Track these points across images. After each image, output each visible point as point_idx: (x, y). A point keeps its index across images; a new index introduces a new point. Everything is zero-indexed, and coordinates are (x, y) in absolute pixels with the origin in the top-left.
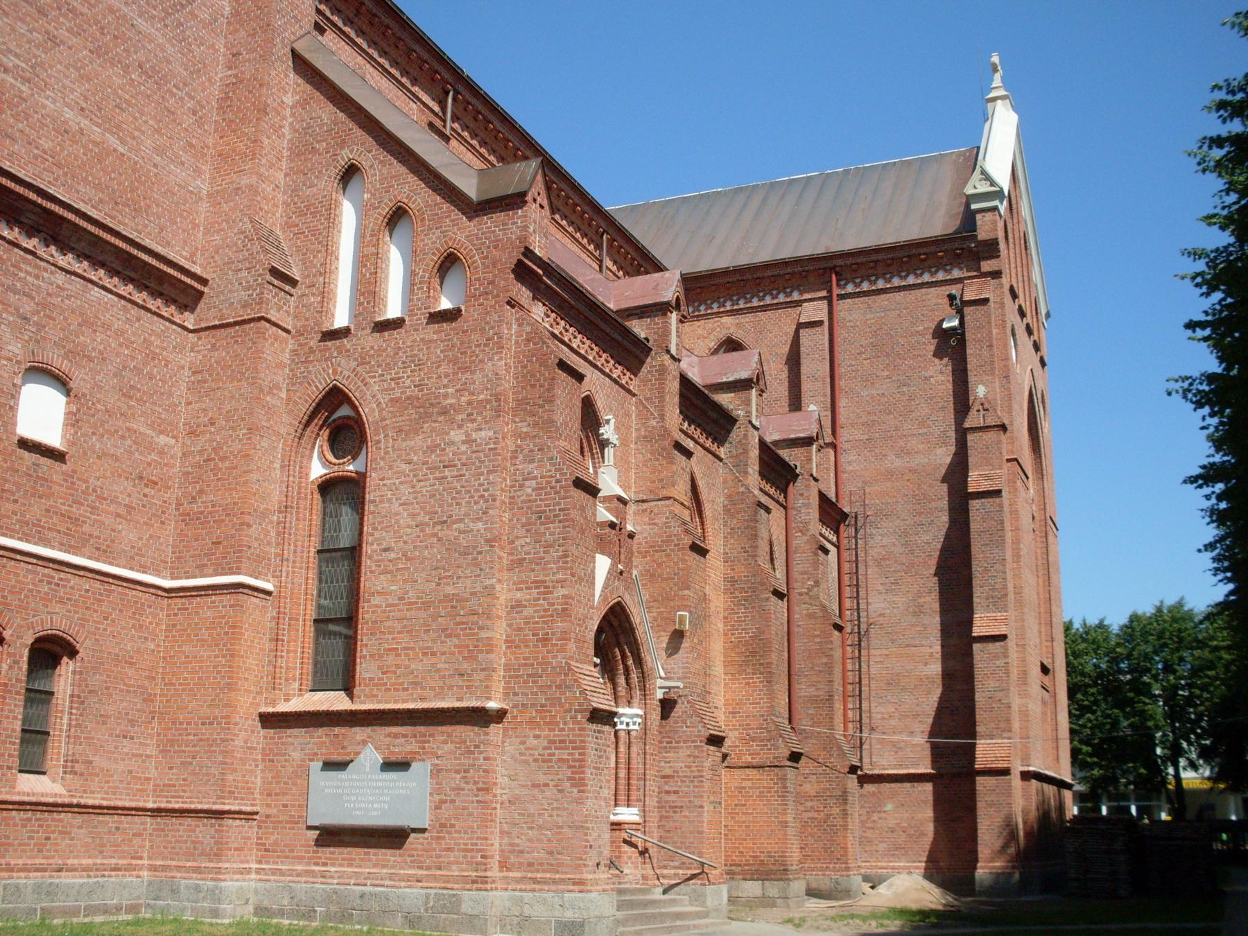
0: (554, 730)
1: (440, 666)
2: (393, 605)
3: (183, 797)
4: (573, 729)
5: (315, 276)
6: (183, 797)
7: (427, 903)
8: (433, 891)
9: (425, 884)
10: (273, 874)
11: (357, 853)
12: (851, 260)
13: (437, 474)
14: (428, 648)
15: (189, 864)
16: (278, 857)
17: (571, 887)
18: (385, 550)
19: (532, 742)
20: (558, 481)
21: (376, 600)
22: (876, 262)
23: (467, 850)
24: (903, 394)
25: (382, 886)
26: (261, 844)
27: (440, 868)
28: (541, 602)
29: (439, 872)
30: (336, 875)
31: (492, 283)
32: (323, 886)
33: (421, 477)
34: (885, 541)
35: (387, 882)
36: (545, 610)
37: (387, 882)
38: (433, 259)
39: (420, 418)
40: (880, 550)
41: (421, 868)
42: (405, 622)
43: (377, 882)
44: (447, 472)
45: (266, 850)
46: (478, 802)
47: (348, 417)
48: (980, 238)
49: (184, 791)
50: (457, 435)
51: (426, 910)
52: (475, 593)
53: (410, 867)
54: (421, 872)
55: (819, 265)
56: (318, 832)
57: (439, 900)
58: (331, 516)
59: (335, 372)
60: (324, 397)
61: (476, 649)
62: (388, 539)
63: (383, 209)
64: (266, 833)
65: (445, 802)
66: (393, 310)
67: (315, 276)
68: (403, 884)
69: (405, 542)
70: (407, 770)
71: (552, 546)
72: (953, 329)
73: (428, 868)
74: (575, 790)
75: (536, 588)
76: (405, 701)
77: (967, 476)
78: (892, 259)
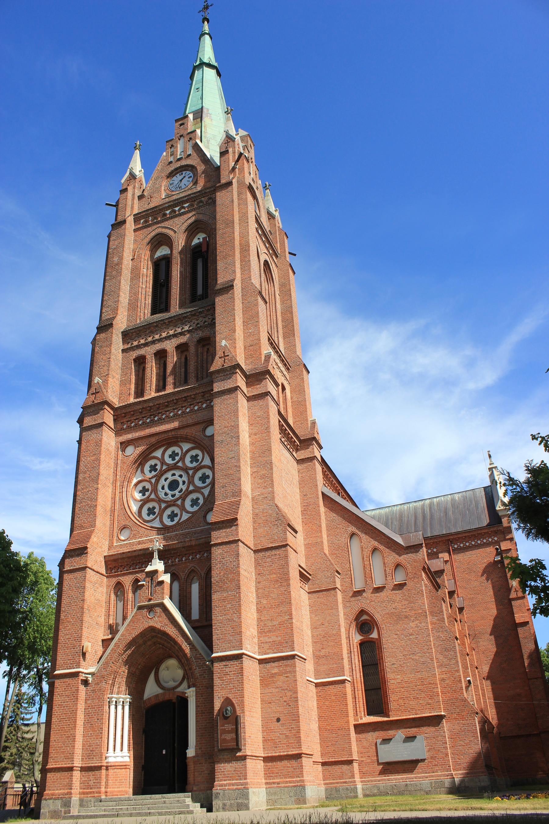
0: (464, 720)
1: (421, 702)
2: (399, 683)
3: (334, 757)
4: (471, 720)
5: (347, 571)
6: (334, 757)
7: (431, 785)
8: (433, 781)
9: (429, 779)
10: (368, 782)
11: (398, 772)
12: (456, 536)
13: (407, 638)
14: (415, 696)
15: (341, 781)
16: (369, 775)
17: (481, 774)
18: (393, 664)
19: (456, 727)
20: (449, 638)
21: (392, 682)
22: (465, 537)
23: (442, 765)
24: (483, 586)
25: (413, 781)
26: (361, 771)
27: (434, 772)
28: (451, 678)
29: (433, 774)
30: (394, 779)
31: (415, 574)
32: (390, 784)
33: (401, 639)
34: (485, 643)
35: (415, 780)
36: (453, 680)
37: (415, 780)
38: (392, 566)
39: (397, 619)
40: (483, 647)
41: (426, 773)
42: (405, 688)
43: (411, 780)
44: (411, 637)
45: (363, 774)
46: (443, 747)
47: (366, 620)
48: (504, 526)
49: (335, 754)
50: (412, 625)
51: (432, 788)
52: (429, 677)
53: (422, 773)
54: (426, 775)
55: (444, 539)
56: (382, 766)
57: (436, 784)
58: (364, 654)
59: (361, 605)
60: (359, 613)
61: (432, 696)
62: (393, 660)
63: (369, 549)
64: (362, 767)
65: (431, 748)
66: (378, 583)
67: (347, 571)
68: (421, 779)
69: (400, 661)
70: (413, 741)
71: (451, 659)
72: (499, 561)
73: (429, 773)
74: (476, 740)
75: (449, 673)
76: (409, 715)
77: (514, 617)
78: (471, 535)
